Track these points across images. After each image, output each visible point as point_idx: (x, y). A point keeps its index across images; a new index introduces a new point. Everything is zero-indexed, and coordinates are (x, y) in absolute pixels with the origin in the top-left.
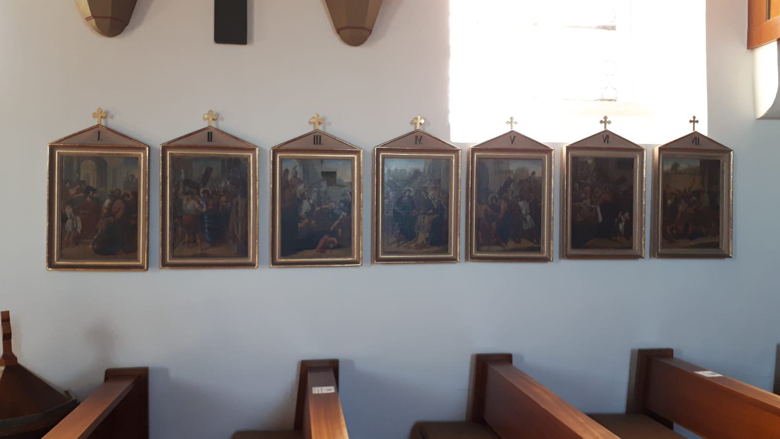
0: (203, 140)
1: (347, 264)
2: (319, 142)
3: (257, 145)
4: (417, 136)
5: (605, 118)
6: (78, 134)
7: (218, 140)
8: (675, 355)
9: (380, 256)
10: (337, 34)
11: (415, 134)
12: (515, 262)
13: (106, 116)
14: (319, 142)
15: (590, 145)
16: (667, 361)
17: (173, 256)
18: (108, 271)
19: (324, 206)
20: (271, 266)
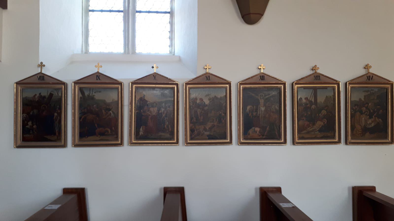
0: (258, 80)
1: (278, 144)
2: (263, 79)
3: (347, 81)
4: (314, 76)
5: (44, 66)
6: (379, 77)
7: (213, 79)
8: (377, 190)
9: (282, 141)
10: (242, 18)
11: (205, 75)
12: (61, 148)
13: (211, 68)
14: (263, 79)
15: (143, 82)
16: (371, 194)
17: (300, 138)
18: (373, 145)
19: (193, 116)
20: (286, 144)
